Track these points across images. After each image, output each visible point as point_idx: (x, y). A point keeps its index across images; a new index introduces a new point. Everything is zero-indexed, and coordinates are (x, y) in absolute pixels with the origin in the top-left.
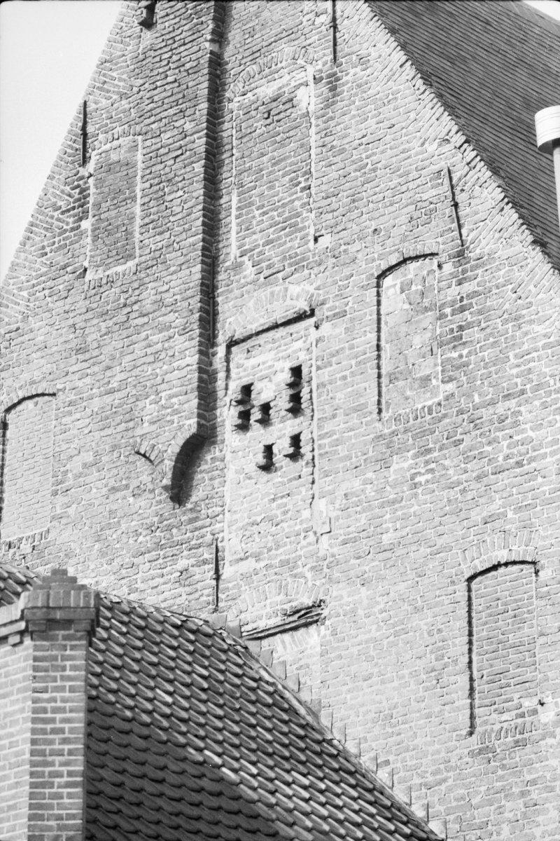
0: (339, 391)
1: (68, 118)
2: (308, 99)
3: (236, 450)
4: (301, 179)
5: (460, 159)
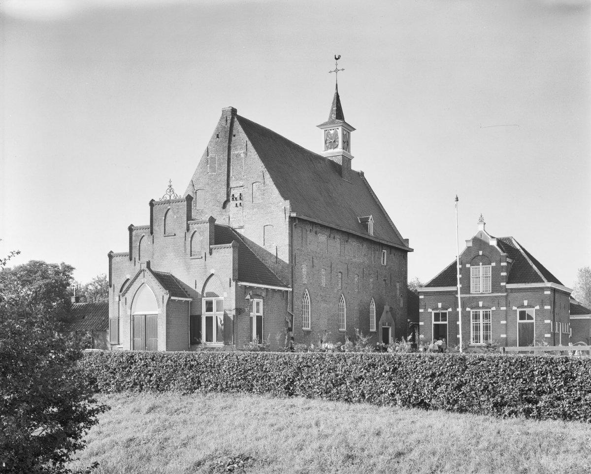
0: (247, 198)
1: (205, 148)
2: (242, 155)
3: (232, 204)
4: (241, 166)
5: (341, 160)
